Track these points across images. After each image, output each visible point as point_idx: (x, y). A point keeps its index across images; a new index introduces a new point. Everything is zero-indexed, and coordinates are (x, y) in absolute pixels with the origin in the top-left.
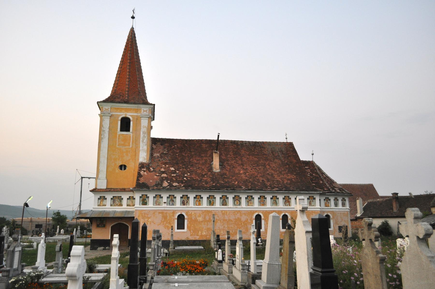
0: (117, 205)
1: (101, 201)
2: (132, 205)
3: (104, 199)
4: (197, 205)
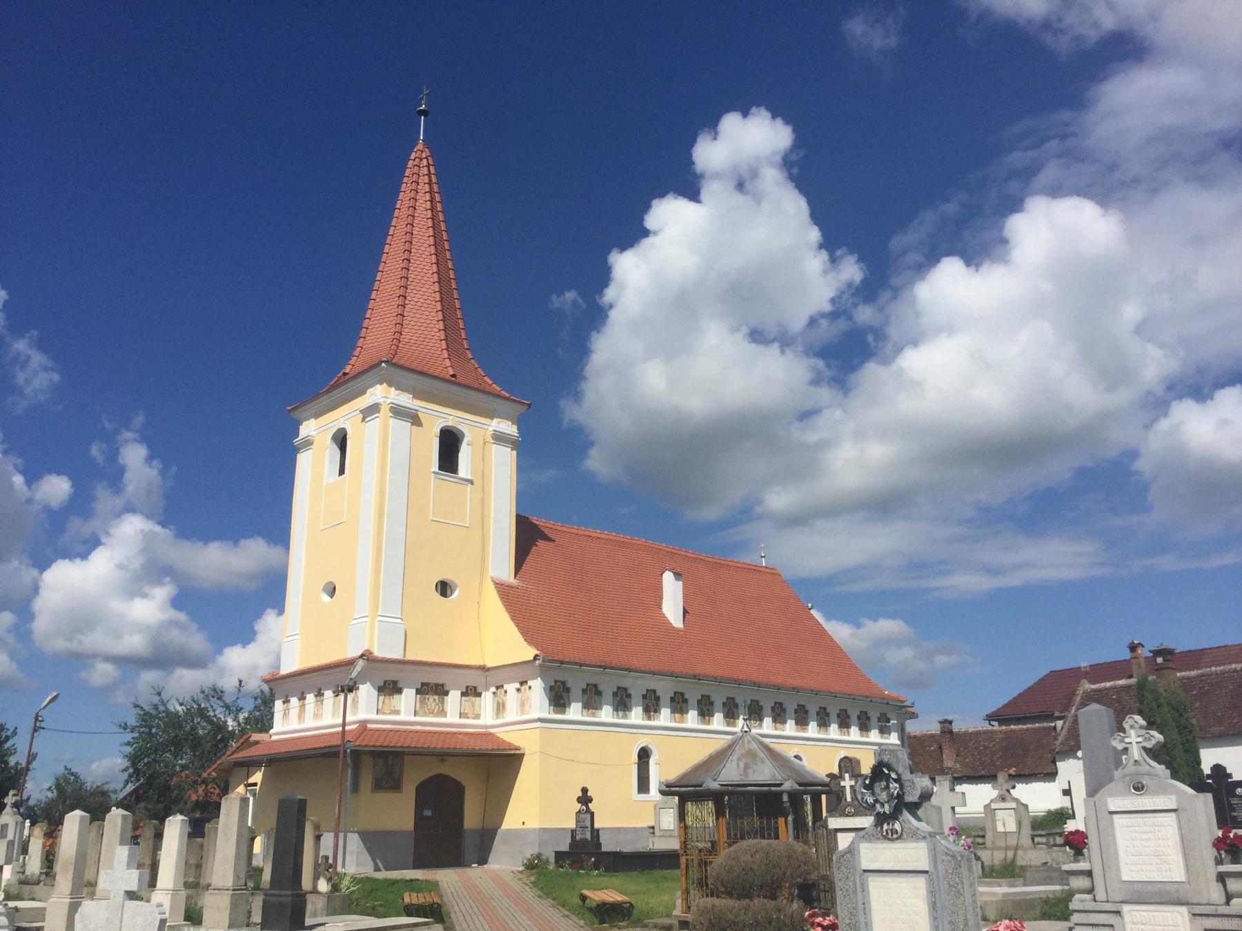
0: (431, 713)
2: (474, 716)
4: (676, 722)
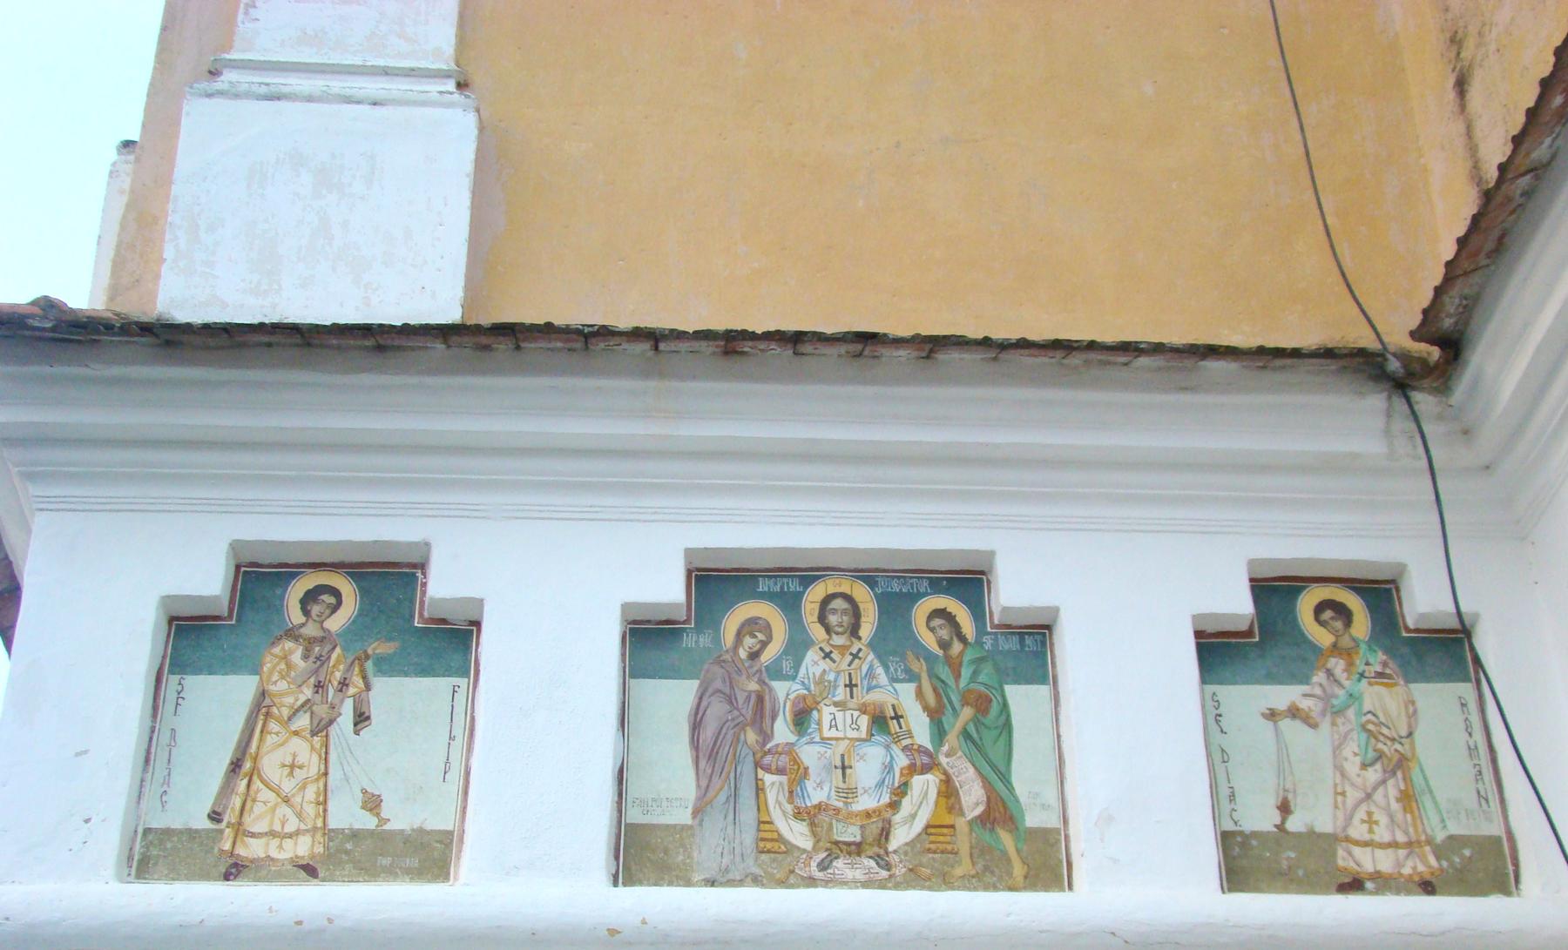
1: (262, 707)
2: (1425, 864)
3: (388, 666)
